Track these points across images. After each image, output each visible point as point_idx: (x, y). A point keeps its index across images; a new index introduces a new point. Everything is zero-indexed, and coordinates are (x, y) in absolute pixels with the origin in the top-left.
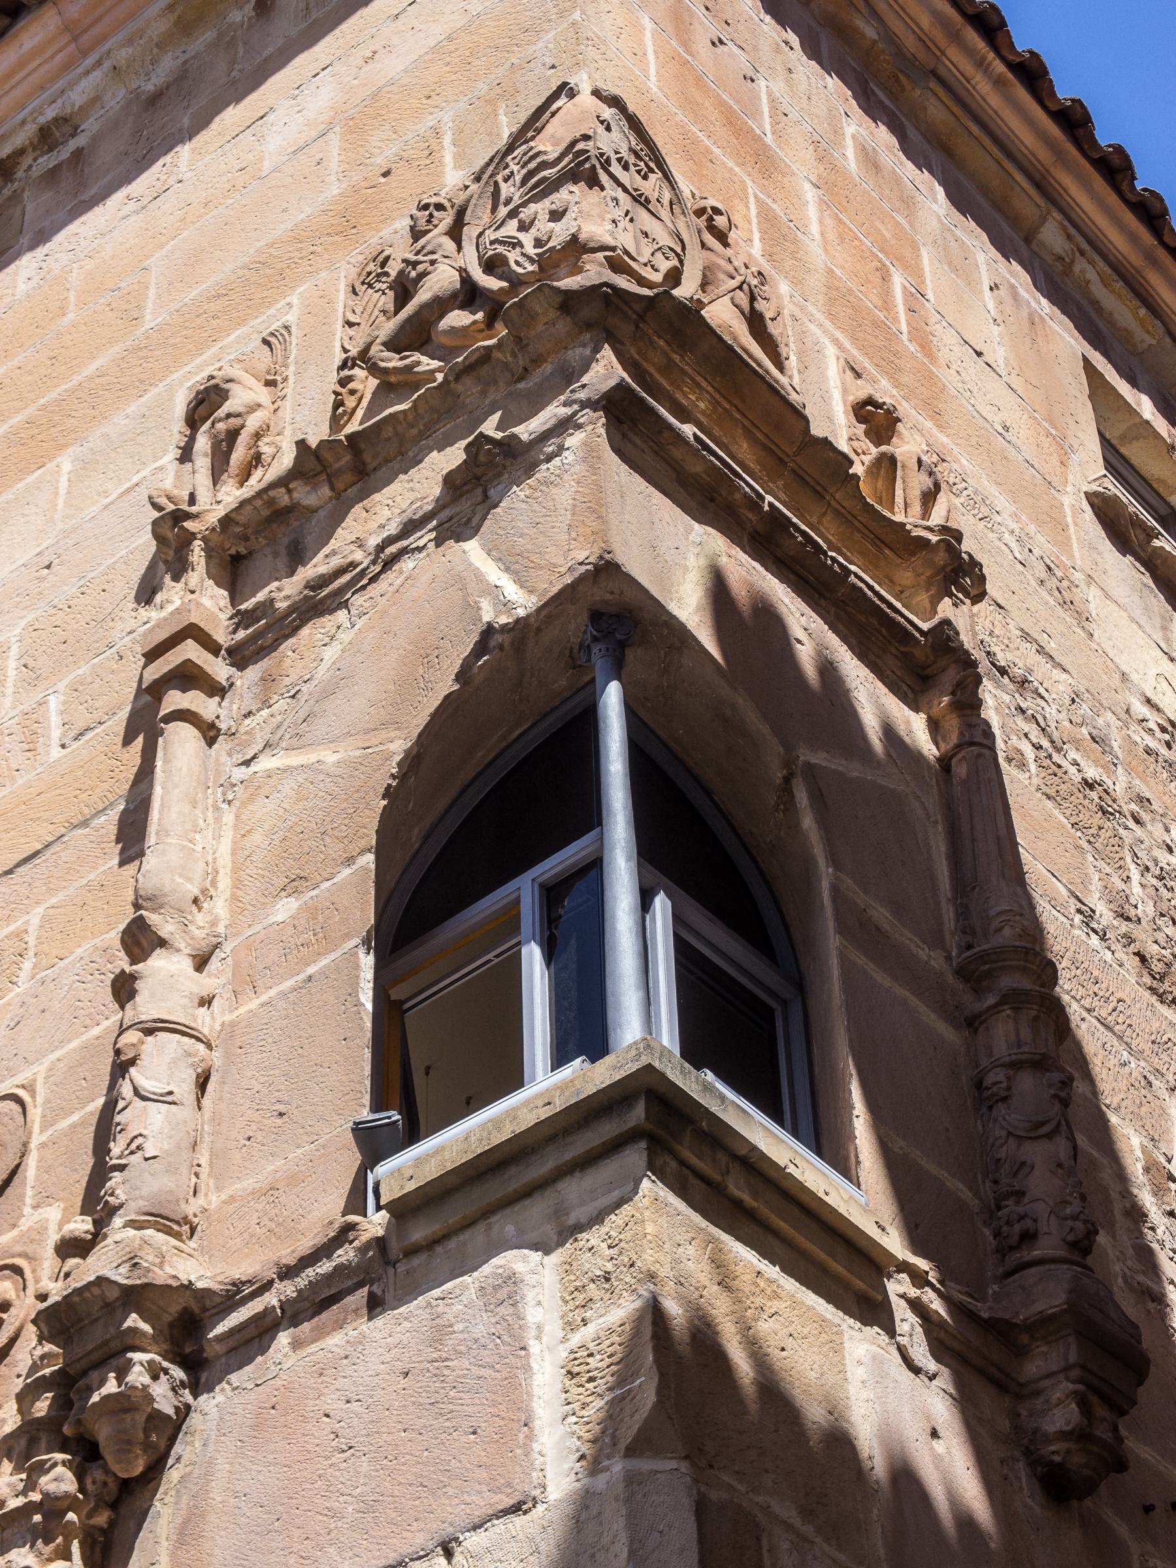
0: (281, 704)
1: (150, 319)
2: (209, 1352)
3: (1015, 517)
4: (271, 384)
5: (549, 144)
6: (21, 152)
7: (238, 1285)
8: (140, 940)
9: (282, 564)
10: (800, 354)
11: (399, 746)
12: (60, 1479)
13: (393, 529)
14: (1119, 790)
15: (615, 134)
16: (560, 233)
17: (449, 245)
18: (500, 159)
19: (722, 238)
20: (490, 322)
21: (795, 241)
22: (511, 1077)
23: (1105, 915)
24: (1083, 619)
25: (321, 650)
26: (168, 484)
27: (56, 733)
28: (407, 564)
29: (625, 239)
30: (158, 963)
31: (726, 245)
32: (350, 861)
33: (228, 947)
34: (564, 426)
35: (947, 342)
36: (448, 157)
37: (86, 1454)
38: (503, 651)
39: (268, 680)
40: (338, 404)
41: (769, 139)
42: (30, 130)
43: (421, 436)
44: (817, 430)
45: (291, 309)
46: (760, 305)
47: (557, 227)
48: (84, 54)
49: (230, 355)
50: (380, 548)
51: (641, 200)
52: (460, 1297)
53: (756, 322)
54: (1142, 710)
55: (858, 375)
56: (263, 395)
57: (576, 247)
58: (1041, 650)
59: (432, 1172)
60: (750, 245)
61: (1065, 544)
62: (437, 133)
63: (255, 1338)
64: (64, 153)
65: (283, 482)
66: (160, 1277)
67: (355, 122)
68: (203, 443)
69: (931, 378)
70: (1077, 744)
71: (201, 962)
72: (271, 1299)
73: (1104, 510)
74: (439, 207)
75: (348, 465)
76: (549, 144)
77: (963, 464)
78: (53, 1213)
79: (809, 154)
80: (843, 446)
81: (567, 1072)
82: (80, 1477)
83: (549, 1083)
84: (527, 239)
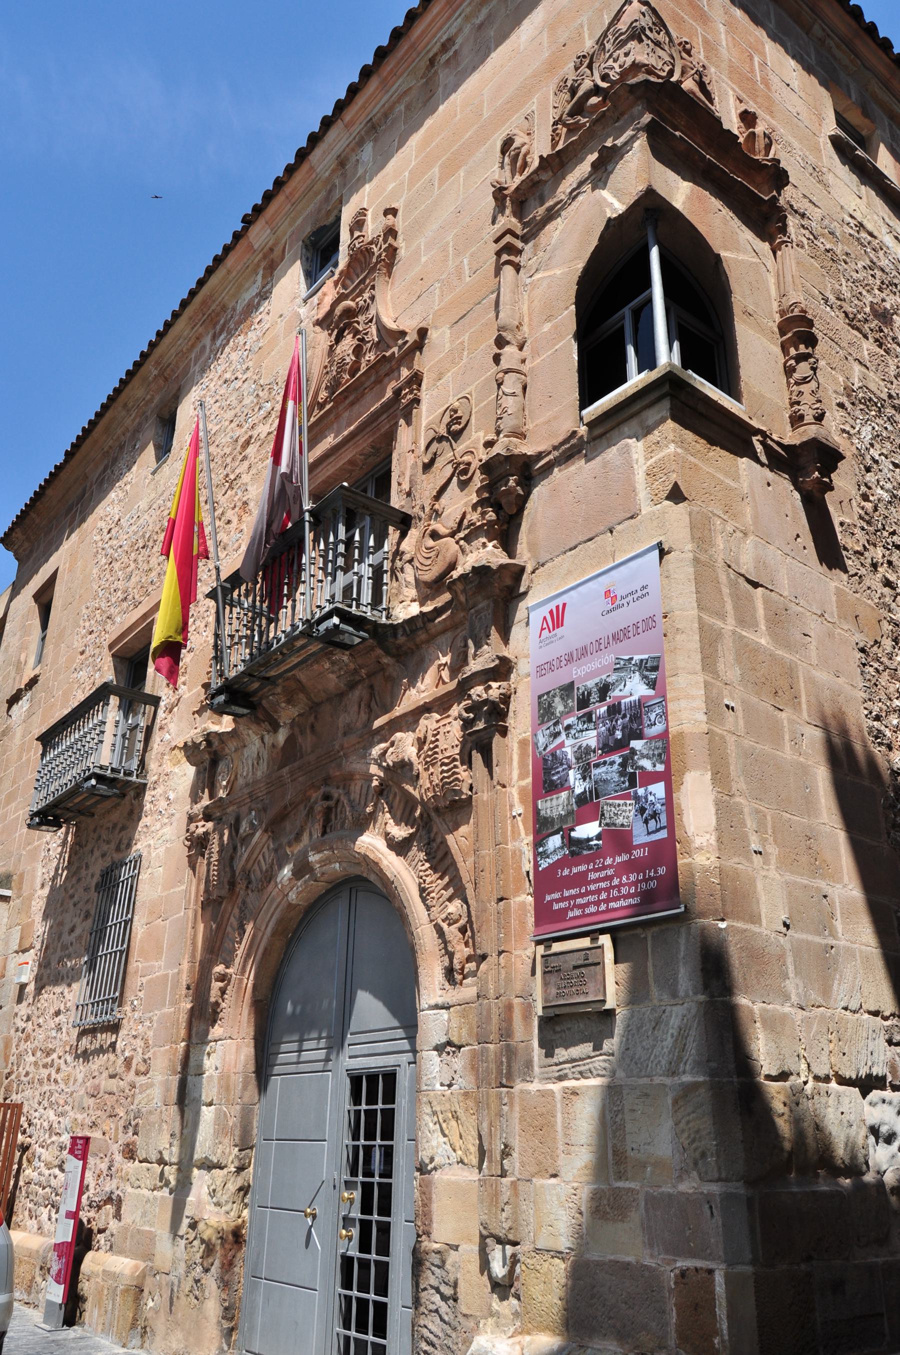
0: (541, 254)
1: (486, 115)
2: (534, 473)
3: (801, 150)
4: (529, 134)
5: (622, 26)
6: (436, 55)
7: (540, 453)
8: (501, 342)
9: (537, 203)
10: (719, 96)
11: (580, 265)
12: (491, 515)
13: (575, 186)
14: (838, 252)
15: (647, 17)
16: (629, 61)
17: (588, 72)
18: (605, 35)
19: (688, 53)
20: (604, 100)
21: (717, 50)
22: (622, 379)
23: (832, 299)
24: (826, 186)
25: (555, 231)
26: (497, 177)
27: (467, 272)
28: (580, 198)
29: (652, 61)
30: (507, 349)
31: (690, 56)
32: (567, 308)
33: (529, 342)
34: (633, 139)
35: (775, 81)
36: (586, 36)
37: (498, 508)
38: (614, 228)
39: (535, 246)
40: (553, 139)
41: (706, 8)
42: (439, 44)
43: (583, 148)
44: (725, 127)
45: (533, 105)
46: (705, 79)
47: (627, 59)
48: (455, 12)
49: (513, 126)
50: (571, 193)
51: (658, 44)
52: (612, 453)
53: (702, 85)
54: (849, 219)
55: (741, 101)
56: (526, 139)
57: (636, 67)
58: (811, 201)
59: (600, 412)
60: (700, 55)
61: (820, 158)
62: (582, 26)
63: (548, 469)
64: (451, 53)
65: (536, 172)
66: (516, 451)
67: (552, 26)
68: (507, 160)
69: (769, 98)
70: (823, 235)
71: (521, 348)
72: (551, 457)
73: (835, 141)
74: (584, 57)
75: (557, 164)
76: (622, 26)
77: (782, 132)
78: (481, 434)
79: (721, 12)
80: (736, 132)
81: (643, 375)
82: (497, 515)
83: (636, 380)
84: (616, 65)
